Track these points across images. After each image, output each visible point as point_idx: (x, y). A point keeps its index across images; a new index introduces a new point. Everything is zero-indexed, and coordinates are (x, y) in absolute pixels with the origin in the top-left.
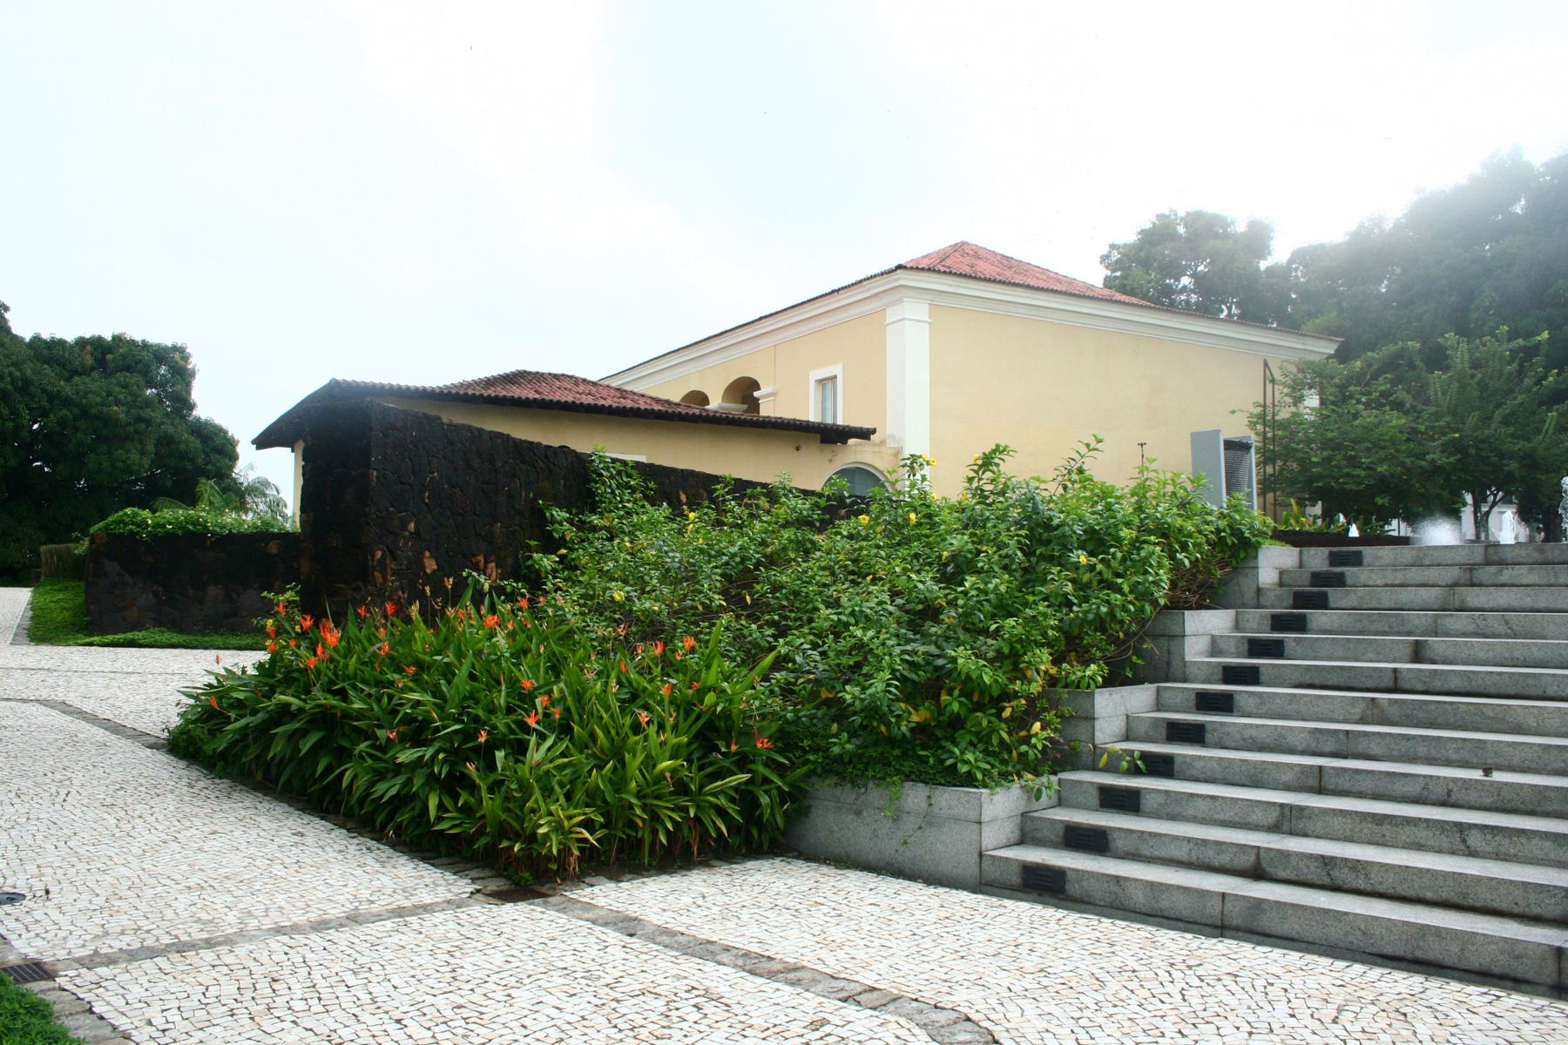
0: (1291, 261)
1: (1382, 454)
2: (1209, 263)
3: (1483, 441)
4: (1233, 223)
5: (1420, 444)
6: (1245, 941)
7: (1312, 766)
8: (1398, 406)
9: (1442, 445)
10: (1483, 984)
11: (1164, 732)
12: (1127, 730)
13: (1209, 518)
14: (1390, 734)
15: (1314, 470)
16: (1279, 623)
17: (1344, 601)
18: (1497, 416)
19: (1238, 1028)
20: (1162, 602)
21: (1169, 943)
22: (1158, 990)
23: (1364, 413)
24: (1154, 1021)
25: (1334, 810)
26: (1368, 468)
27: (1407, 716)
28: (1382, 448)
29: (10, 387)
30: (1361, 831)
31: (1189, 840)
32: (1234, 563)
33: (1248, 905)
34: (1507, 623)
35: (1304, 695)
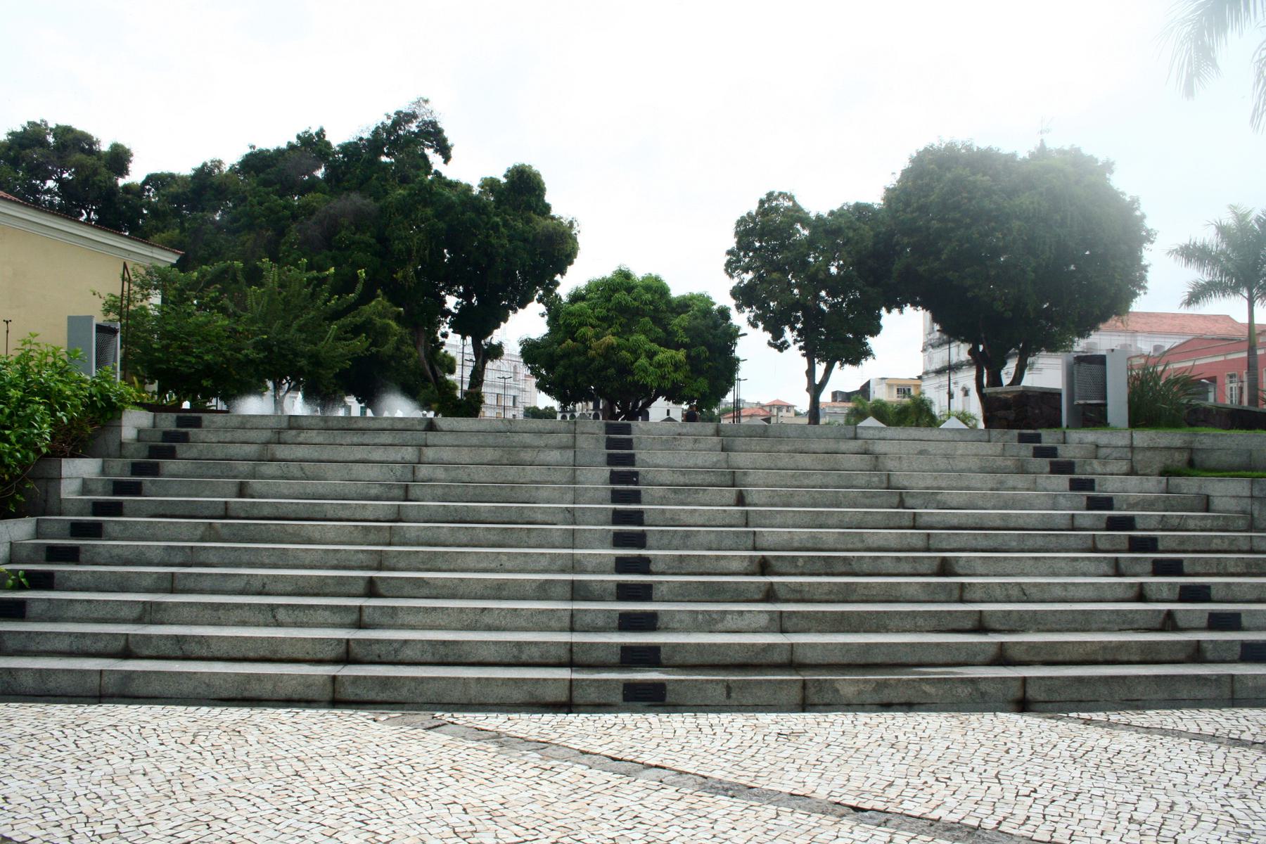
0: (145, 183)
1: (209, 346)
2: (73, 173)
3: (284, 343)
4: (98, 142)
5: (238, 341)
6: (119, 703)
7: (166, 573)
8: (223, 310)
9: (254, 343)
10: (288, 707)
11: (44, 555)
12: (11, 555)
13: (84, 385)
14: (223, 548)
15: (157, 354)
16: (137, 469)
17: (188, 453)
18: (295, 325)
19: (123, 758)
20: (44, 450)
21: (57, 713)
22: (55, 744)
23: (196, 313)
24: (55, 764)
25: (184, 603)
26: (197, 357)
27: (234, 535)
28: (209, 341)
30: (203, 616)
31: (70, 634)
32: (102, 422)
33: (121, 676)
34: (302, 469)
35: (159, 522)
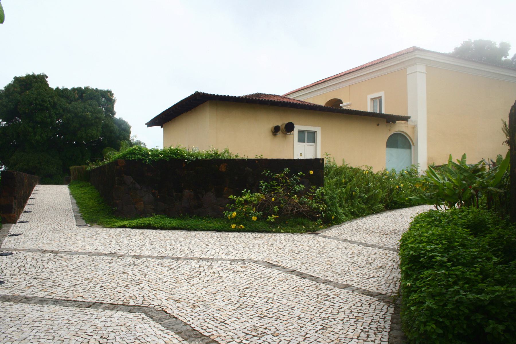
29: (49, 106)
